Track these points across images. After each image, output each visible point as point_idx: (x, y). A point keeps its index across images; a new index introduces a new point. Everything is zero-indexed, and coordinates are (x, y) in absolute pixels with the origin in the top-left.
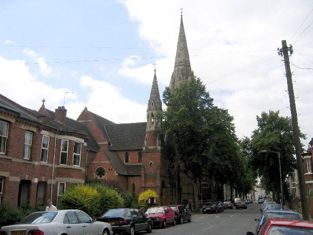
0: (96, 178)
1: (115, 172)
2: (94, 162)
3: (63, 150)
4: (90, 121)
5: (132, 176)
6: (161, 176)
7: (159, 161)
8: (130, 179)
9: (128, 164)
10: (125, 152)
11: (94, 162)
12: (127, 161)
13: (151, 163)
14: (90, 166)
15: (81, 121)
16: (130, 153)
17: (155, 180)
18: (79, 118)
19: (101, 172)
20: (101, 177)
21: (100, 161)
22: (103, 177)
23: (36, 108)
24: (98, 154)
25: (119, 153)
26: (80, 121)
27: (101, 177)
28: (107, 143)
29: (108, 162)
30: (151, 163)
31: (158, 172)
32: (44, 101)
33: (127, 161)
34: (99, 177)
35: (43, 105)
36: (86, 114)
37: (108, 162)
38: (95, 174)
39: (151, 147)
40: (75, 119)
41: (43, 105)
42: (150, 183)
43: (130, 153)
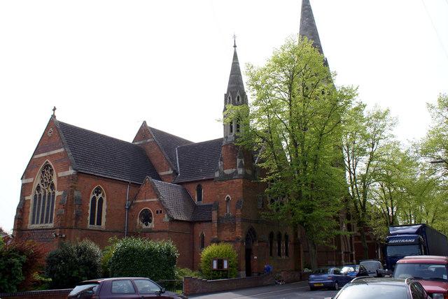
0: (141, 227)
1: (166, 215)
2: (138, 201)
3: (355, 240)
4: (149, 140)
5: (200, 222)
6: (243, 220)
7: (240, 195)
8: (197, 226)
9: (202, 203)
10: (197, 184)
11: (138, 201)
12: (200, 199)
13: (228, 198)
14: (132, 207)
15: (141, 142)
16: (203, 185)
17: (233, 227)
18: (134, 141)
19: (147, 218)
20: (147, 225)
21: (145, 199)
22: (151, 225)
23: (127, 134)
24: (143, 188)
25: (187, 187)
26: (136, 143)
27: (147, 225)
28: (171, 172)
29: (155, 200)
30: (228, 198)
31: (239, 213)
32: (54, 109)
33: (200, 199)
34: (144, 226)
35: (54, 116)
36: (145, 131)
37: (155, 200)
38: (138, 219)
39: (228, 172)
40: (131, 142)
41: (54, 116)
42: (227, 234)
43: (203, 185)
